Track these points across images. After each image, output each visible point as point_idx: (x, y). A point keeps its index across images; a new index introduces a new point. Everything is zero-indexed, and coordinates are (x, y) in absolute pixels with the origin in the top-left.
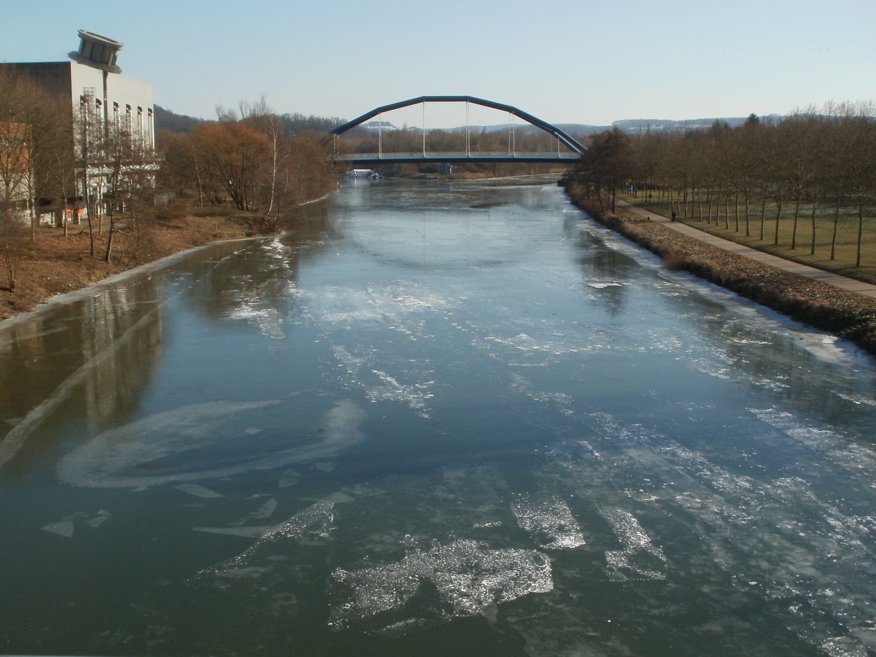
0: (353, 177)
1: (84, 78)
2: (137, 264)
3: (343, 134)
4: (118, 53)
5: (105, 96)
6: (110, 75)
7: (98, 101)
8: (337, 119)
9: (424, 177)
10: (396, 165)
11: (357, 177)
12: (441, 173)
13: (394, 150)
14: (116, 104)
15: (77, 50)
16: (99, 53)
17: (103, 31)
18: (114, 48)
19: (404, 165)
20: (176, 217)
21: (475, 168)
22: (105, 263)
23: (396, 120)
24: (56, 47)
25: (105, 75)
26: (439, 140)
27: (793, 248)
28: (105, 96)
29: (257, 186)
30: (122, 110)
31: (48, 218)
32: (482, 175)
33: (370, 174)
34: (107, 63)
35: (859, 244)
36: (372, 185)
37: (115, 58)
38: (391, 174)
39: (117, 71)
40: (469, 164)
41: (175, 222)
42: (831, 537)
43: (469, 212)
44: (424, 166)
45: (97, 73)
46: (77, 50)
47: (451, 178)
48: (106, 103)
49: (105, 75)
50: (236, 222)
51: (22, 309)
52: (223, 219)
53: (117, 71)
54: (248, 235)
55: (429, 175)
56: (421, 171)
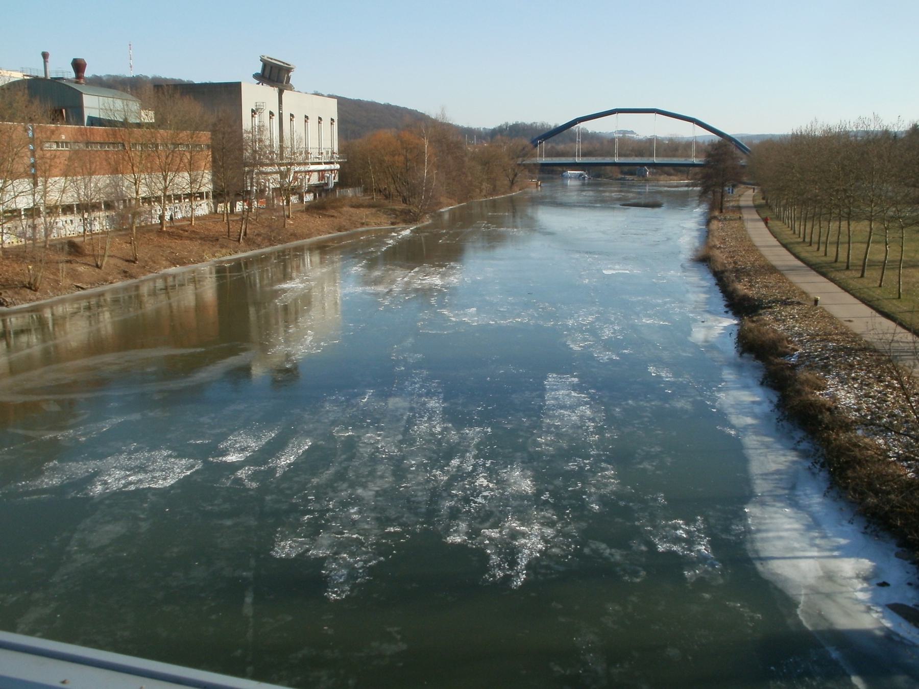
0: (567, 178)
1: (255, 95)
2: (271, 245)
3: (550, 140)
4: (291, 74)
5: (280, 108)
6: (286, 93)
7: (271, 114)
8: (507, 124)
9: (623, 179)
10: (603, 168)
11: (570, 178)
12: (639, 176)
13: (625, 156)
14: (292, 115)
15: (260, 72)
16: (274, 75)
17: (279, 56)
18: (289, 70)
19: (608, 168)
20: (333, 208)
21: (672, 171)
22: (237, 244)
23: (590, 127)
24: (240, 69)
25: (281, 93)
26: (646, 147)
27: (811, 245)
28: (280, 108)
29: (417, 182)
30: (299, 122)
31: (221, 208)
32: (675, 178)
33: (581, 175)
34: (282, 82)
35: (849, 243)
36: (583, 185)
37: (289, 78)
38: (599, 176)
39: (291, 88)
40: (666, 169)
41: (332, 212)
42: (666, 526)
43: (618, 208)
44: (626, 169)
45: (274, 91)
46: (260, 72)
47: (647, 180)
48: (281, 115)
49: (281, 93)
50: (385, 213)
51: (132, 277)
52: (374, 210)
53: (291, 88)
54: (393, 224)
55: (628, 177)
56: (622, 173)
